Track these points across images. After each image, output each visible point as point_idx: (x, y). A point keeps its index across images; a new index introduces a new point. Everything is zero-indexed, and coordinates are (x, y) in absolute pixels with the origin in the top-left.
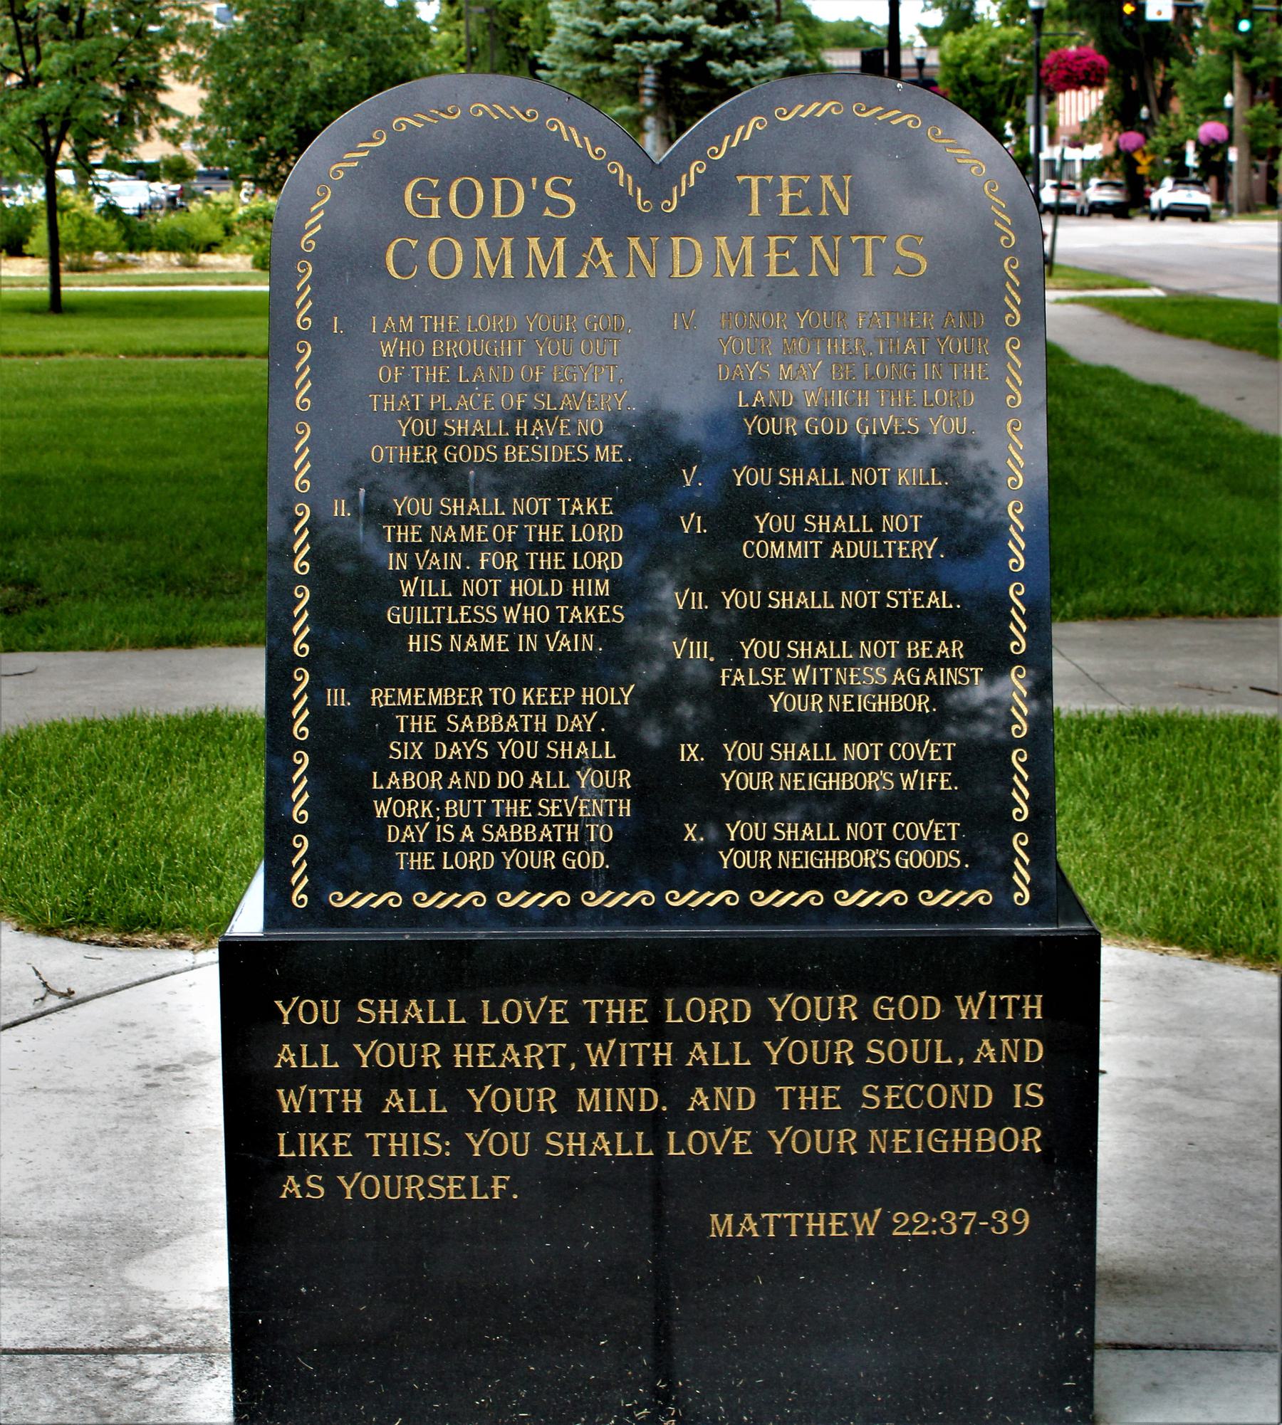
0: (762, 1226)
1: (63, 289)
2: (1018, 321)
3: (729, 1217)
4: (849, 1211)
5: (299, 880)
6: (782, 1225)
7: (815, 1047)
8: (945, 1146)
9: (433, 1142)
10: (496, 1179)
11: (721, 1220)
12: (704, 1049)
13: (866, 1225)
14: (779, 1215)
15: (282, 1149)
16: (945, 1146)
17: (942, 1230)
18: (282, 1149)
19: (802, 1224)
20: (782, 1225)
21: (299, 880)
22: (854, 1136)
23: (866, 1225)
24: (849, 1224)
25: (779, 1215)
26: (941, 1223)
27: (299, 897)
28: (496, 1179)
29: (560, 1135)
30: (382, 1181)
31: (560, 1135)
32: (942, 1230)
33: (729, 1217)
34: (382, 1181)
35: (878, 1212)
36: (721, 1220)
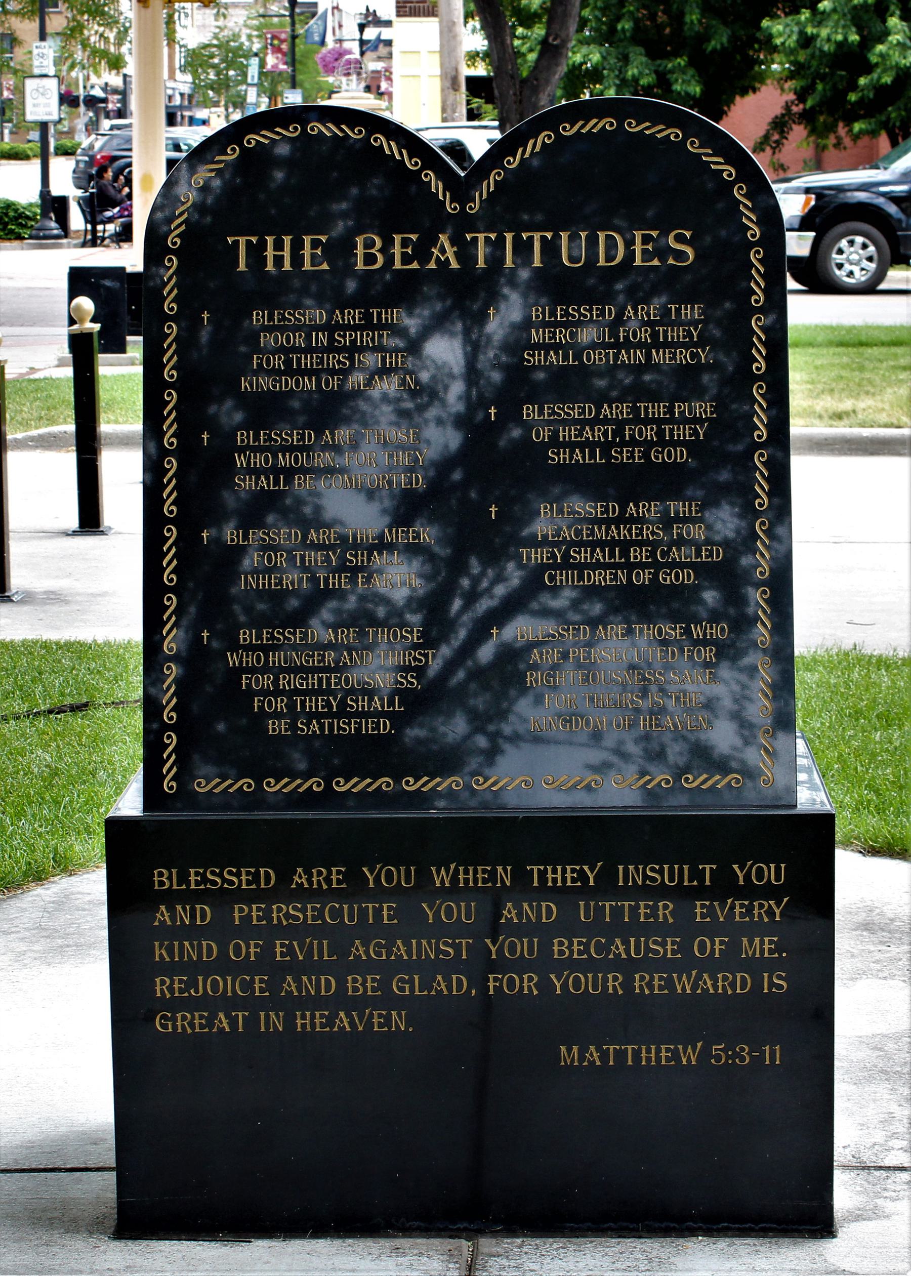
0: (604, 1056)
1: (71, 428)
2: (765, 507)
3: (575, 1049)
4: (676, 1044)
5: (169, 769)
6: (621, 1055)
7: (773, 870)
8: (407, 989)
9: (210, 948)
10: (192, 871)
11: (569, 1050)
12: (404, 946)
13: (690, 1056)
14: (618, 1047)
15: (323, 990)
16: (407, 989)
17: (737, 1060)
18: (323, 990)
19: (637, 1054)
20: (621, 1055)
21: (169, 769)
22: (621, 979)
23: (690, 1056)
24: (676, 1056)
25: (618, 1047)
26: (736, 1055)
27: (168, 785)
28: (192, 871)
29: (657, 867)
30: (586, 978)
31: (657, 867)
32: (737, 1060)
33: (575, 1049)
34: (586, 978)
35: (699, 1045)
36: (569, 1050)
